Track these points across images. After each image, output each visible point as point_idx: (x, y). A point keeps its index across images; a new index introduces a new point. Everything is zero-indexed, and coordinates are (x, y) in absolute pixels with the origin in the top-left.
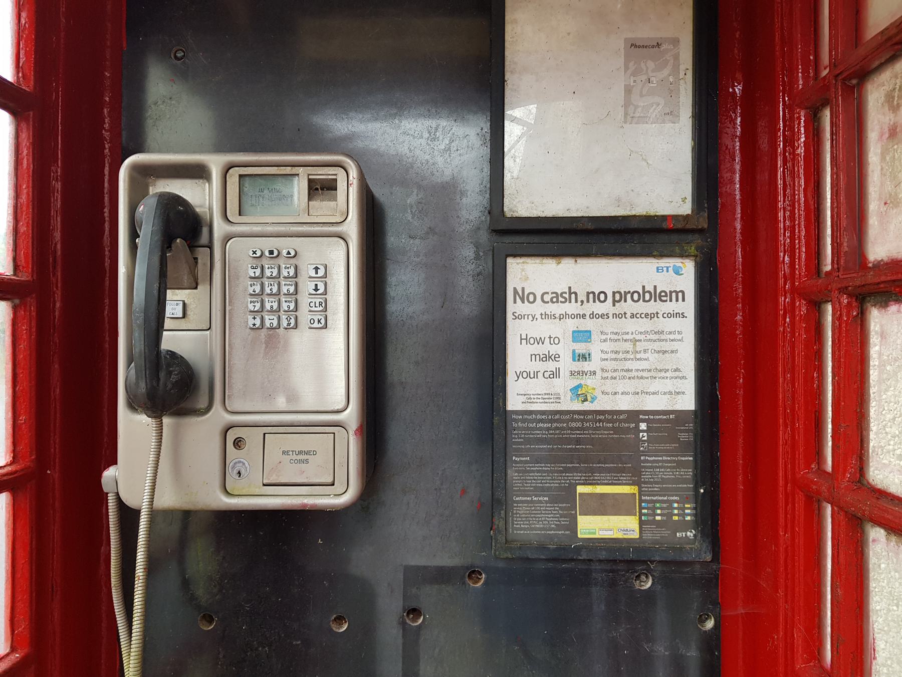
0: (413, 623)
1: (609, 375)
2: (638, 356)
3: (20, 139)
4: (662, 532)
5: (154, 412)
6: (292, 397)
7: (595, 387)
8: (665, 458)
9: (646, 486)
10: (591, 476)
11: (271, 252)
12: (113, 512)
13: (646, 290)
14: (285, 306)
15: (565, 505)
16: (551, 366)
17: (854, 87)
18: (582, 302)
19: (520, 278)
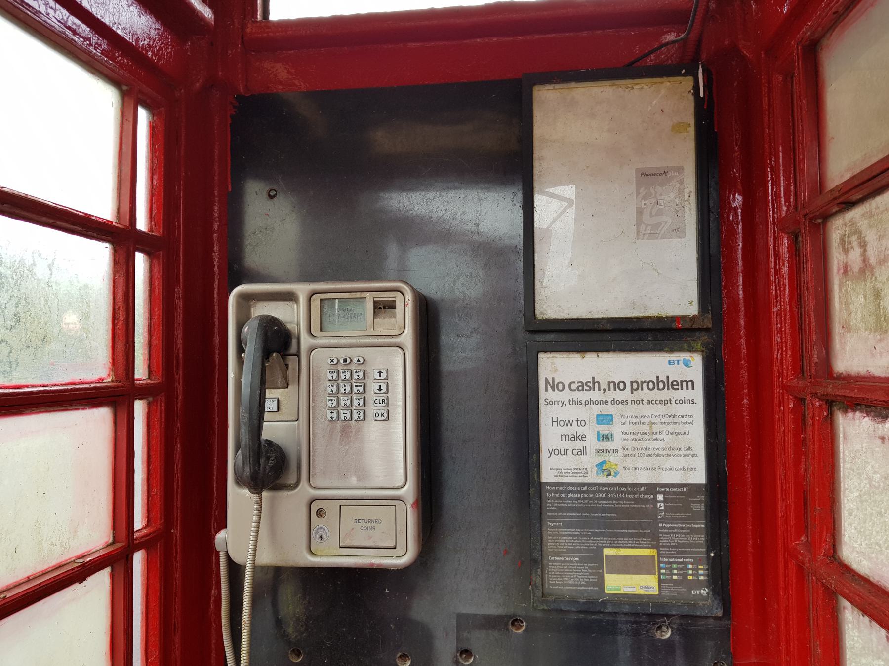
0: (465, 662)
1: (630, 453)
2: (654, 437)
3: (152, 273)
4: (679, 590)
5: (255, 490)
6: (362, 473)
7: (617, 463)
8: (680, 525)
9: (664, 549)
10: (615, 540)
11: (345, 360)
12: (223, 566)
13: (660, 380)
14: (355, 403)
15: (593, 565)
16: (579, 445)
17: (820, 224)
18: (604, 390)
19: (551, 370)
